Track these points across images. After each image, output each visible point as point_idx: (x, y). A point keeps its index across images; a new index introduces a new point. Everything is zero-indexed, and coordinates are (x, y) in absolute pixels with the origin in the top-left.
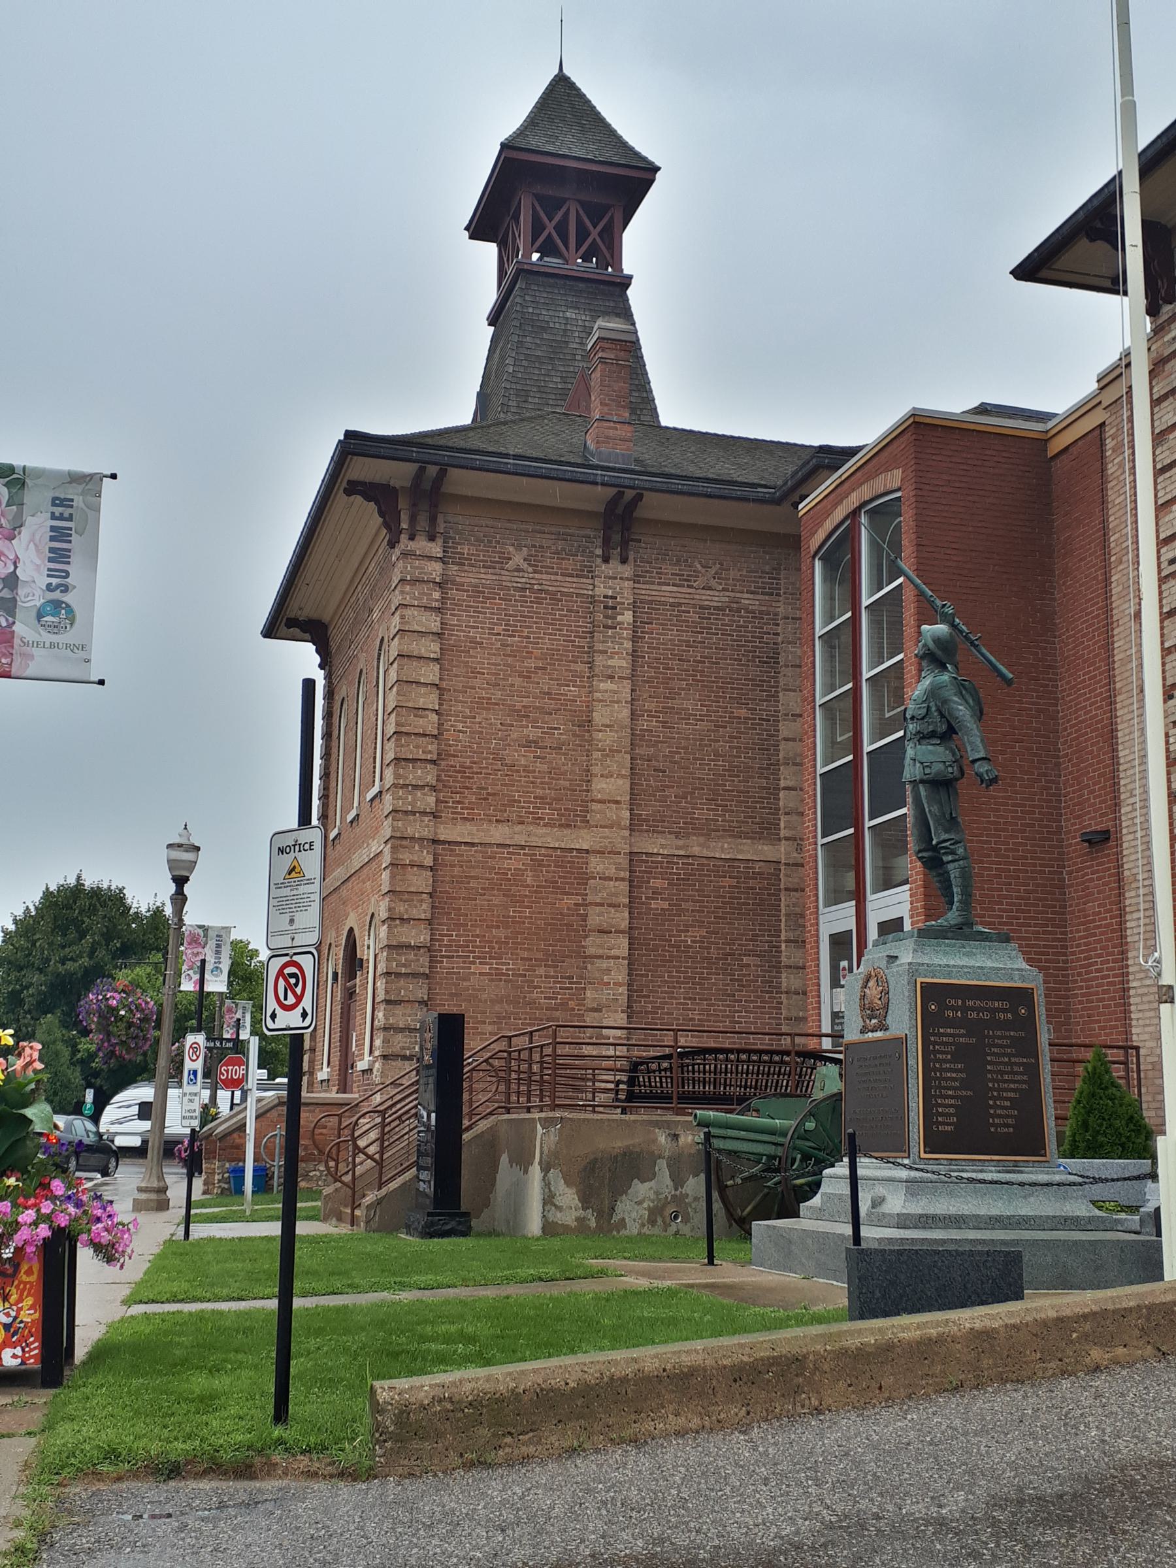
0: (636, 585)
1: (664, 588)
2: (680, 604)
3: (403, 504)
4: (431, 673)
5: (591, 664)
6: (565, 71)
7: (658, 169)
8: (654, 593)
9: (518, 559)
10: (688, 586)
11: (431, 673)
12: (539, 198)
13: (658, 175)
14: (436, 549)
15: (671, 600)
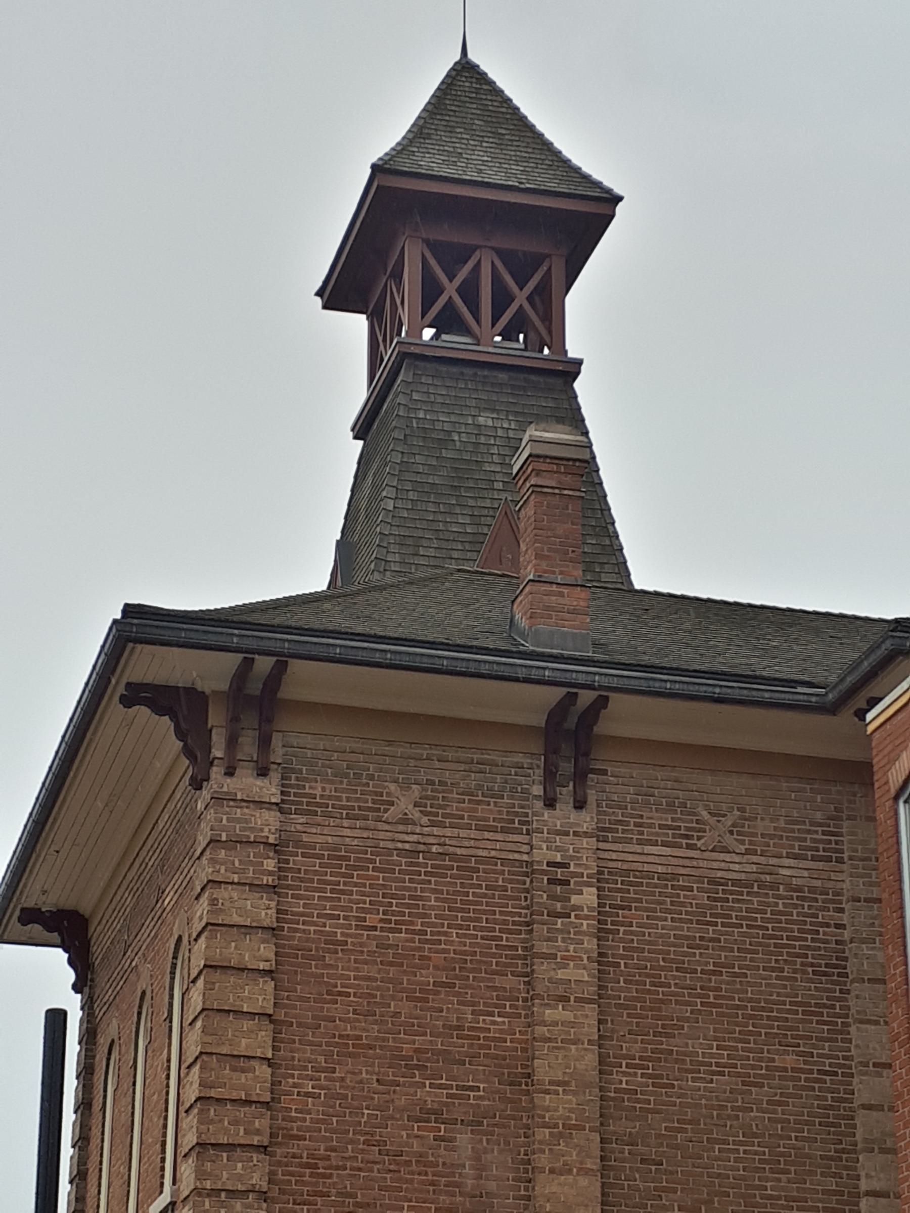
0: (602, 845)
1: (648, 849)
2: (675, 876)
3: (216, 718)
4: (259, 996)
5: (529, 977)
6: (471, 56)
7: (620, 199)
8: (630, 857)
9: (404, 804)
10: (690, 847)
11: (259, 996)
12: (433, 246)
13: (620, 208)
15: (660, 869)
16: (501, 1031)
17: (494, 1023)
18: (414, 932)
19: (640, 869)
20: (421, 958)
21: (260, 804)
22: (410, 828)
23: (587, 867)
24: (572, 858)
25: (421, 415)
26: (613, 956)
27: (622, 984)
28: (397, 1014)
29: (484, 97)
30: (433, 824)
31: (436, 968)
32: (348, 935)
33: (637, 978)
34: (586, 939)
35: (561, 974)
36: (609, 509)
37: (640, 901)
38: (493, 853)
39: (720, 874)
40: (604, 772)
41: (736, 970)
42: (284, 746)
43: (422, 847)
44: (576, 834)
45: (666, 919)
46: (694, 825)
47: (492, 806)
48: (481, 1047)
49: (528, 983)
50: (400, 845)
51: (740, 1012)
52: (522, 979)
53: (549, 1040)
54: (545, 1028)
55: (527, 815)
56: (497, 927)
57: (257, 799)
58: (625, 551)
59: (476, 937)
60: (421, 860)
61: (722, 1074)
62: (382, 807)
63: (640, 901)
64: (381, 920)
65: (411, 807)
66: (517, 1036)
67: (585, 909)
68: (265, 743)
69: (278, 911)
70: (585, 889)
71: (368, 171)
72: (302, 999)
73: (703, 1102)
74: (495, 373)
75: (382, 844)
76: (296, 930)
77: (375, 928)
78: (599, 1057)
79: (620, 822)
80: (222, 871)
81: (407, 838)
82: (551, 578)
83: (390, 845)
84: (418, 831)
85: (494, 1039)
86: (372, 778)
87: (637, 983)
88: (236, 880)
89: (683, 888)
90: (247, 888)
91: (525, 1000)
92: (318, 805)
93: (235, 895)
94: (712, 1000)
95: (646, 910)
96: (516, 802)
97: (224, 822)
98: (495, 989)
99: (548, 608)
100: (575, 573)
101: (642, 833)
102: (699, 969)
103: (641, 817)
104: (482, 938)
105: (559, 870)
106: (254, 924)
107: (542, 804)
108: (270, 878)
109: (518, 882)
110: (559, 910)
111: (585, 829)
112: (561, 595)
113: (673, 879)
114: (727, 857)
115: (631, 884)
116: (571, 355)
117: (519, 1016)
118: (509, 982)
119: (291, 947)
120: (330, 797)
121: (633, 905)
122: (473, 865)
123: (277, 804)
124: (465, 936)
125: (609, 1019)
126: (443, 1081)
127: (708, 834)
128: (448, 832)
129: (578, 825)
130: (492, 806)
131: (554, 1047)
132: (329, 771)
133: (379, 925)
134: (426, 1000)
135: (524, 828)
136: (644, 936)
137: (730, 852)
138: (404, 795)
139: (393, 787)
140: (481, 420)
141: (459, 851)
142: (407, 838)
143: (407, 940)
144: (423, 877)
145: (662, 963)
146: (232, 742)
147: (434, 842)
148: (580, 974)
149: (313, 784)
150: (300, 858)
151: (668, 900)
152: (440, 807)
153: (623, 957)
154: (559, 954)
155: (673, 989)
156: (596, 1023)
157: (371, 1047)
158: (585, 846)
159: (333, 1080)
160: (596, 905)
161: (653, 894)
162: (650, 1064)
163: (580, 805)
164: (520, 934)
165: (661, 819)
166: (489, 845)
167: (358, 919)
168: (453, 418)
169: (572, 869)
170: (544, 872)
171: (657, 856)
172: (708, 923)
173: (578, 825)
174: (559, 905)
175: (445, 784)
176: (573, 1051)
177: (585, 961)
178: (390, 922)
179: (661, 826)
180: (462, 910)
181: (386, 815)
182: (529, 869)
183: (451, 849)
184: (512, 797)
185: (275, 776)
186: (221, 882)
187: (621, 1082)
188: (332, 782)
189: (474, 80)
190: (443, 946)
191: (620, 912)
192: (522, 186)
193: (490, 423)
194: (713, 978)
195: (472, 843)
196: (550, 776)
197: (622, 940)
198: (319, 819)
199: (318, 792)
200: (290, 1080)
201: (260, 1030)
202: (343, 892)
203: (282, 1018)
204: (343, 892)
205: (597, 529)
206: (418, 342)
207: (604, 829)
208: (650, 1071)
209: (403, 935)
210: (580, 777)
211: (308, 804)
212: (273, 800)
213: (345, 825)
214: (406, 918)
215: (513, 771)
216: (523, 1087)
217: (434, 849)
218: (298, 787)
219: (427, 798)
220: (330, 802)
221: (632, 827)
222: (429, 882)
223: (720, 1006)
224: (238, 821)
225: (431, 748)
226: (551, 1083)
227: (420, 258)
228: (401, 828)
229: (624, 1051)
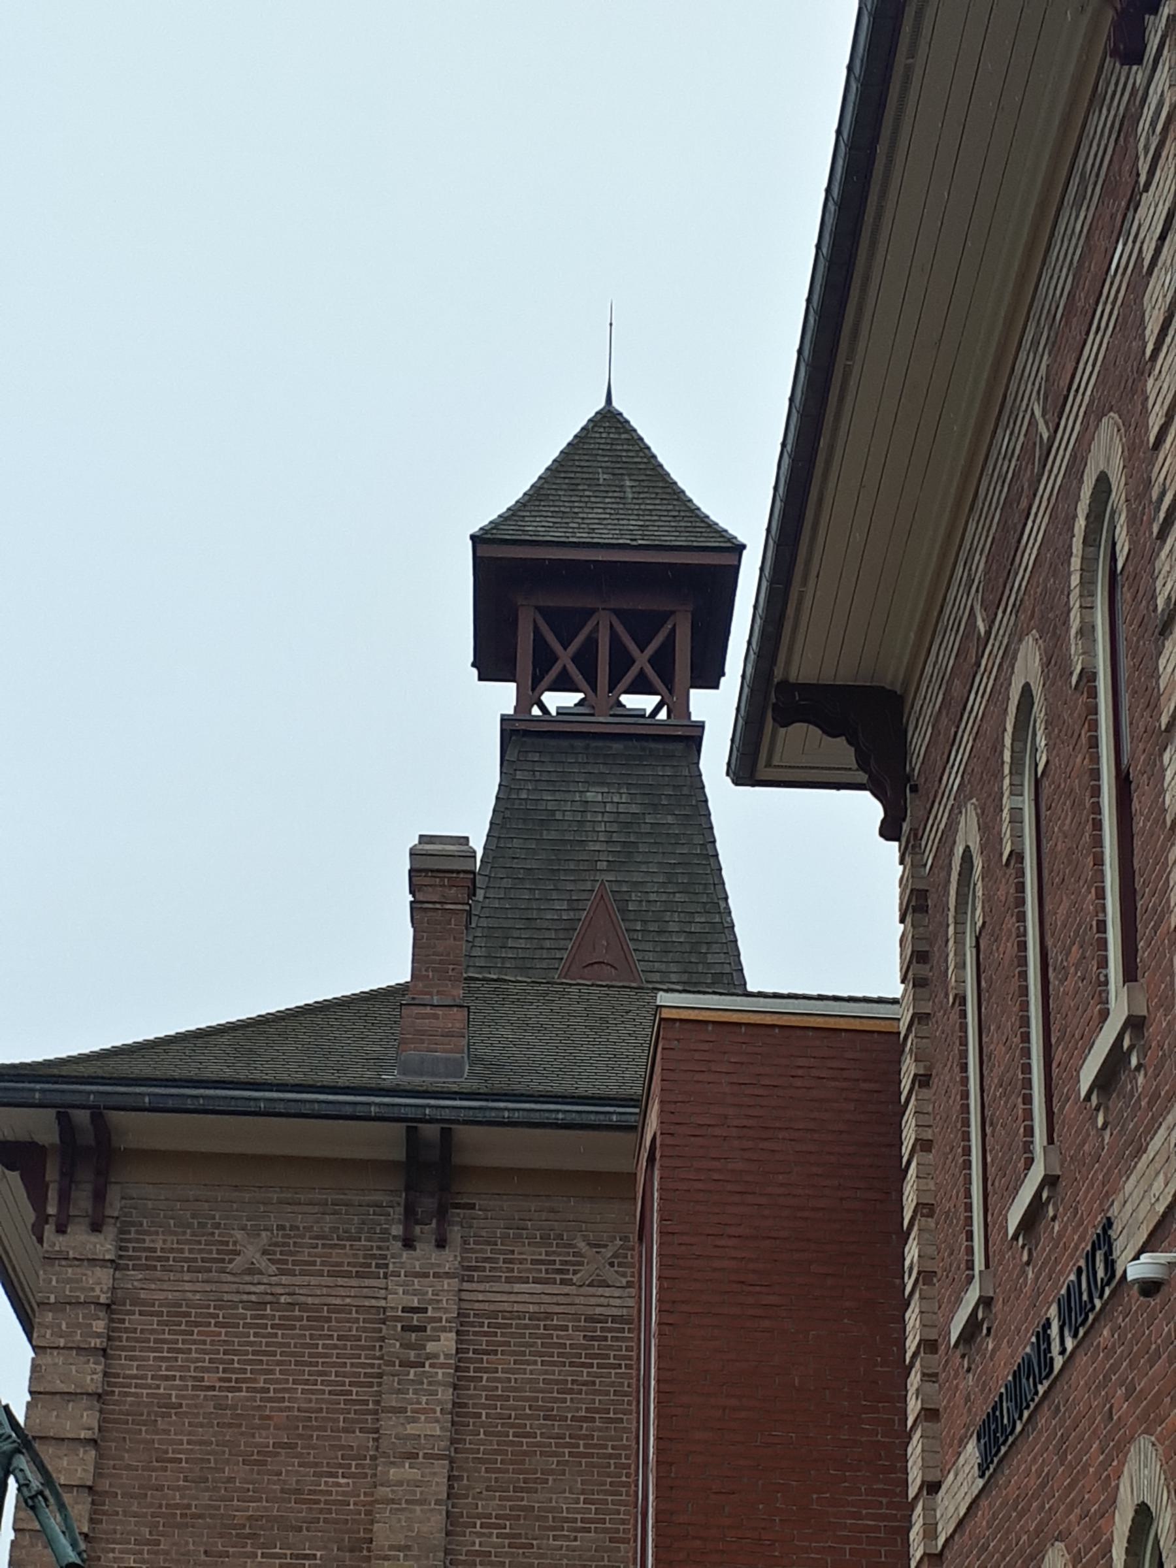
0: (466, 1286)
1: (518, 1287)
2: (549, 1316)
3: (52, 1173)
8: (499, 1297)
9: (251, 1253)
10: (563, 1282)
14: (104, 1245)
15: (531, 1308)
16: (344, 1494)
17: (338, 1485)
18: (255, 1390)
19: (509, 1309)
20: (262, 1418)
21: (93, 1261)
22: (256, 1278)
23: (446, 1310)
24: (431, 1302)
25: (524, 796)
26: (475, 1405)
27: (482, 1436)
28: (231, 1480)
29: (619, 447)
30: (282, 1272)
31: (277, 1428)
32: (184, 1397)
33: (499, 1428)
34: (440, 1389)
35: (411, 1429)
36: (723, 884)
37: (508, 1344)
38: (348, 1300)
39: (598, 1310)
40: (472, 1207)
41: (611, 1415)
42: (123, 1198)
43: (269, 1298)
44: (436, 1275)
45: (535, 1363)
46: (571, 1258)
47: (348, 1250)
48: (321, 1511)
49: (376, 1440)
50: (245, 1297)
51: (612, 1461)
52: (371, 1435)
53: (393, 1501)
54: (388, 1489)
55: (385, 1257)
56: (347, 1380)
57: (90, 1257)
58: (736, 929)
59: (323, 1392)
60: (268, 1311)
61: (588, 1530)
62: (227, 1258)
63: (508, 1344)
64: (221, 1380)
65: (258, 1255)
66: (362, 1498)
67: (442, 1357)
68: (99, 1197)
69: (106, 1374)
70: (443, 1336)
71: (470, 543)
72: (128, 1467)
73: (565, 1562)
74: (608, 744)
75: (226, 1297)
76: (127, 1394)
77: (213, 1388)
78: (448, 1517)
79: (486, 1260)
80: (48, 1336)
81: (253, 1289)
82: (426, 999)
83: (236, 1298)
84: (265, 1281)
85: (335, 1502)
86: (218, 1226)
87: (499, 1434)
88: (62, 1345)
89: (556, 1328)
90: (75, 1352)
91: (373, 1458)
92: (159, 1259)
93: (60, 1361)
94: (582, 1449)
95: (514, 1353)
96: (374, 1244)
97: (54, 1283)
98: (342, 1447)
99: (423, 1033)
100: (455, 992)
101: (512, 1270)
102: (570, 1416)
103: (513, 1252)
104: (330, 1393)
105: (415, 1316)
106: (78, 1391)
107: (400, 1244)
108: (98, 1341)
109: (374, 1330)
110: (412, 1359)
111: (447, 1270)
112: (436, 1016)
113: (546, 1319)
114: (607, 1291)
115: (499, 1326)
116: (694, 718)
117: (365, 1476)
118: (357, 1439)
119: (121, 1413)
120: (172, 1250)
121: (500, 1349)
122: (325, 1314)
123: (112, 1261)
124: (312, 1392)
125: (465, 1475)
126: (277, 1550)
127: (586, 1267)
128: (298, 1280)
129: (439, 1265)
130: (348, 1250)
131: (398, 1509)
132: (172, 1222)
133: (218, 1385)
134: (264, 1463)
135: (382, 1271)
136: (510, 1382)
137: (609, 1286)
138: (252, 1244)
139: (239, 1235)
140: (590, 796)
141: (310, 1300)
142: (253, 1289)
143: (248, 1399)
144: (269, 1330)
145: (528, 1411)
146: (64, 1198)
147: (282, 1291)
148: (431, 1429)
149: (154, 1237)
150: (137, 1316)
151: (539, 1341)
152: (291, 1253)
153: (484, 1406)
154: (409, 1407)
155: (538, 1439)
156: (445, 1480)
157: (200, 1516)
158: (446, 1287)
159: (156, 1553)
160: (454, 1352)
161: (523, 1336)
162: (508, 1523)
163: (441, 1244)
164: (372, 1387)
165: (534, 1253)
166: (342, 1292)
167: (195, 1378)
168: (558, 796)
169: (429, 1314)
170: (397, 1319)
171: (526, 1295)
172: (583, 1365)
173: (439, 1265)
174: (412, 1353)
175: (298, 1228)
176: (418, 1512)
177: (438, 1414)
178: (230, 1380)
179: (533, 1262)
180: (311, 1364)
181: (231, 1266)
182: (383, 1316)
183: (302, 1299)
184: (369, 1240)
185: (110, 1231)
186: (45, 1348)
187: (474, 1544)
188: (175, 1233)
189: (613, 430)
190: (287, 1404)
191: (485, 1357)
192: (634, 543)
193: (599, 798)
194: (585, 1425)
195: (325, 1291)
196: (410, 1216)
197: (485, 1388)
198: (158, 1274)
199: (159, 1245)
200: (111, 1555)
201: (77, 1503)
202: (180, 1351)
203: (107, 1488)
204: (180, 1351)
205: (708, 906)
206: (528, 718)
207: (469, 1268)
208: (507, 1531)
209: (243, 1394)
210: (442, 1214)
211: (147, 1258)
212: (107, 1257)
213: (185, 1278)
214: (249, 1375)
215: (371, 1210)
216: (365, 1553)
217: (283, 1299)
218: (138, 1241)
219: (276, 1244)
220: (171, 1255)
221: (501, 1264)
222: (276, 1335)
223: (592, 1455)
224: (69, 1281)
225: (282, 1192)
226: (391, 1548)
227: (531, 628)
228: (247, 1278)
229: (480, 1510)
